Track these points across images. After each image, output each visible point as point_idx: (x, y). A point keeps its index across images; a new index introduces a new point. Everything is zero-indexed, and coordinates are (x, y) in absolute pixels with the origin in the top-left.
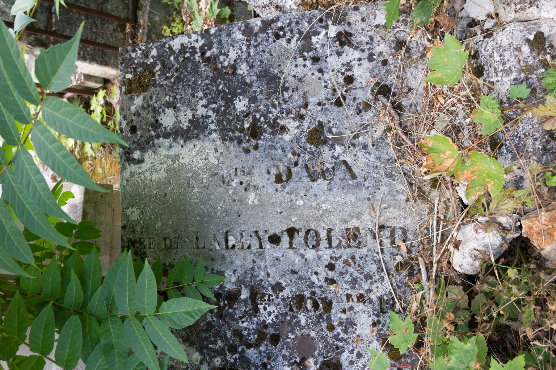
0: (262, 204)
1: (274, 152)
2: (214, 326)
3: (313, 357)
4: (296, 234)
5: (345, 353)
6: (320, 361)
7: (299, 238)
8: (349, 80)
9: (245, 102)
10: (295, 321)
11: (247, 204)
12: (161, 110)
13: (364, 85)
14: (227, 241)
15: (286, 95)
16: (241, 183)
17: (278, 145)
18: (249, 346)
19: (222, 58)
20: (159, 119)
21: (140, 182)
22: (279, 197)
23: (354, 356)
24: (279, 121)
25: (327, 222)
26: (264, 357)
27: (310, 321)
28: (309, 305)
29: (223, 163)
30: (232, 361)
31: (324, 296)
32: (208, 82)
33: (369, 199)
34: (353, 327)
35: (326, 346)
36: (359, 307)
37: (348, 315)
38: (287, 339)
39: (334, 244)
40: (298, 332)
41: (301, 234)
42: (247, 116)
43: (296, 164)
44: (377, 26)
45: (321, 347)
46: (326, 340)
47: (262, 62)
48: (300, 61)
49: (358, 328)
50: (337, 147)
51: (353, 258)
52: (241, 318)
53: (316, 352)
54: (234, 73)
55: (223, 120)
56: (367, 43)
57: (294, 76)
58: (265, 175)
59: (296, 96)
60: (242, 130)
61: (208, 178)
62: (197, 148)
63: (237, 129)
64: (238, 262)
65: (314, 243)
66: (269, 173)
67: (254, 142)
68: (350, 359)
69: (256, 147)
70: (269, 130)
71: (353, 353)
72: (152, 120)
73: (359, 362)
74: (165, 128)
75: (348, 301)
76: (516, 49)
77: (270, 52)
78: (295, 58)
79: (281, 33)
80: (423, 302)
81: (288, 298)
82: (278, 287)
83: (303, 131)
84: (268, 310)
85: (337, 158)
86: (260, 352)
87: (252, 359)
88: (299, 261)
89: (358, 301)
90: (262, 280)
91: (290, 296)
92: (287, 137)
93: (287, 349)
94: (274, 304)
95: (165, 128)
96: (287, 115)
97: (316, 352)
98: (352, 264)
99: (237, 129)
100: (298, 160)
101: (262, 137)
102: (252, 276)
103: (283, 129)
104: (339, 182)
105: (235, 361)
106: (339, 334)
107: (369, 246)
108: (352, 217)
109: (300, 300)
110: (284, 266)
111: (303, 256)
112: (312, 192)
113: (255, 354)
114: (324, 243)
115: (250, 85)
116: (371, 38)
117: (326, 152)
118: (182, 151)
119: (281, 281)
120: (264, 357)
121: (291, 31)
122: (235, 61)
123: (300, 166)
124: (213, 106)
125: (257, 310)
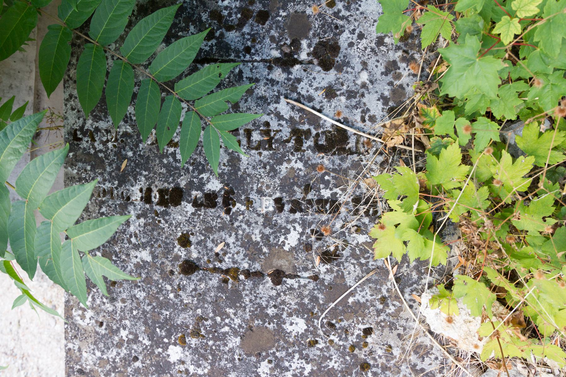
2: (186, 8)
3: (307, 38)
5: (345, 33)
6: (315, 42)
18: (230, 28)
23: (355, 36)
26: (248, 40)
30: (207, 48)
34: (357, 3)
35: (323, 25)
38: (277, 17)
45: (317, 26)
46: (324, 18)
49: (362, 4)
53: (311, 33)
68: (350, 40)
71: (354, 34)
73: (360, 44)
80: (547, 370)
86: (243, 34)
87: (233, 43)
93: (276, 29)
97: (311, 33)
105: (211, 49)
106: (339, 11)
113: (237, 37)
120: (248, 40)
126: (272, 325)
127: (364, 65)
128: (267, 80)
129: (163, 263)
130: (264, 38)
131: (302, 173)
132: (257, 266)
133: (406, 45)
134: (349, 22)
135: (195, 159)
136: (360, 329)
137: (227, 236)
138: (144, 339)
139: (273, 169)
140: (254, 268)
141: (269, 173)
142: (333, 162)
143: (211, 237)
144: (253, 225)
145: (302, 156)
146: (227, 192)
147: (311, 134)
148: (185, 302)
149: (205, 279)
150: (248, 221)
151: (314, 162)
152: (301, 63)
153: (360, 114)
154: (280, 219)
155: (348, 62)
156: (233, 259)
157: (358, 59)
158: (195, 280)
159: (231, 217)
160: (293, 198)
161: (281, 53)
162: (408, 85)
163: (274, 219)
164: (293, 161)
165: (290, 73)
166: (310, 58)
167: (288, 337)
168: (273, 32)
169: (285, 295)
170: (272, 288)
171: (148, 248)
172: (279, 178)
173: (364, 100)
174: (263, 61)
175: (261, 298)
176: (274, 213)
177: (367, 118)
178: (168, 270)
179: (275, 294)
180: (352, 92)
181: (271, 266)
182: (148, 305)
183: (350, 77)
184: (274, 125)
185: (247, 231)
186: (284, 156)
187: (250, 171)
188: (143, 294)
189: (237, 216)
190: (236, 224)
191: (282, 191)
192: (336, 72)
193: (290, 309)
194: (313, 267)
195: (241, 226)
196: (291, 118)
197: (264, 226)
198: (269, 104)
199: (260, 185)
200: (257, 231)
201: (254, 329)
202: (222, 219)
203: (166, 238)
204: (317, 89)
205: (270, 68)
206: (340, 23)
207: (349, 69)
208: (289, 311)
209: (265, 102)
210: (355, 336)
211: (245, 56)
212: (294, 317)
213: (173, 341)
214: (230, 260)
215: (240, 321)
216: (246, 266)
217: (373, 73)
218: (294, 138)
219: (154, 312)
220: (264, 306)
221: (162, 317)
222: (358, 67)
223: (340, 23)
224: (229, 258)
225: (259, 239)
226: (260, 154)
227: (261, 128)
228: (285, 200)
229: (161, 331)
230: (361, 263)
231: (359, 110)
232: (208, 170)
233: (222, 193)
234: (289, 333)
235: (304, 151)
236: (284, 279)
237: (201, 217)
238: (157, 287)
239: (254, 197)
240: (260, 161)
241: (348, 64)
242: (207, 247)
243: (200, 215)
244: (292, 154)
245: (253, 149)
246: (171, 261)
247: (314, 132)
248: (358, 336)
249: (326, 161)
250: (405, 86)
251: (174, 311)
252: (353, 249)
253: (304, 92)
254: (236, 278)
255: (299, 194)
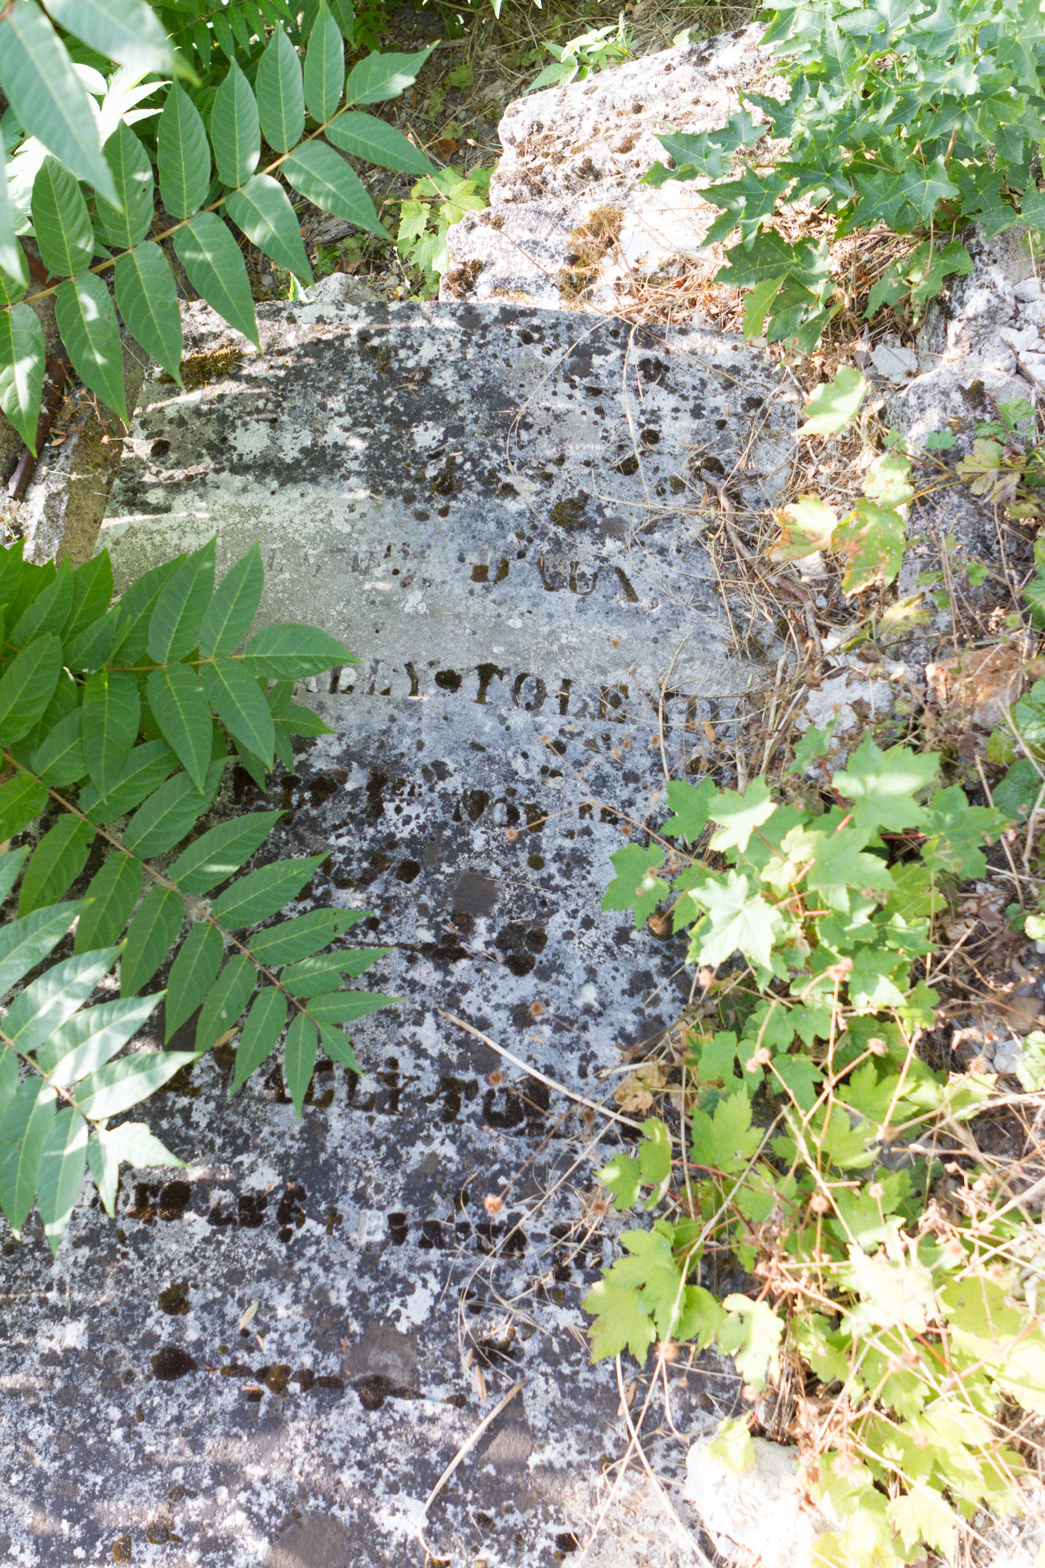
0: (434, 612)
1: (479, 525)
3: (487, 915)
4: (496, 677)
7: (501, 687)
8: (651, 437)
9: (439, 433)
10: (460, 840)
11: (398, 612)
12: (239, 422)
13: (677, 451)
14: (336, 679)
15: (525, 436)
16: (396, 572)
17: (492, 515)
19: (403, 353)
20: (231, 437)
21: (149, 548)
22: (475, 605)
24: (501, 475)
25: (567, 666)
26: (376, 906)
27: (494, 844)
28: (499, 814)
29: (361, 532)
31: (532, 801)
32: (362, 388)
33: (655, 641)
35: (519, 898)
36: (603, 831)
37: (577, 843)
39: (573, 707)
40: (463, 862)
41: (506, 678)
42: (437, 456)
43: (521, 555)
44: (716, 367)
47: (487, 372)
48: (564, 387)
50: (609, 542)
51: (607, 739)
52: (335, 827)
54: (425, 381)
55: (381, 457)
56: (694, 388)
57: (548, 409)
58: (454, 563)
59: (544, 441)
60: (420, 479)
61: (319, 557)
62: (309, 499)
63: (408, 477)
64: (352, 718)
65: (531, 699)
66: (461, 559)
67: (440, 503)
68: (567, 928)
69: (444, 512)
70: (478, 486)
72: (213, 437)
74: (241, 456)
75: (582, 817)
76: (943, 393)
77: (507, 361)
78: (555, 380)
79: (536, 336)
81: (454, 794)
82: (438, 770)
83: (546, 501)
84: (404, 813)
85: (604, 560)
88: (493, 728)
89: (603, 820)
90: (402, 755)
91: (461, 791)
92: (512, 506)
94: (422, 803)
95: (241, 456)
96: (519, 468)
98: (603, 749)
99: (408, 477)
100: (526, 549)
101: (461, 496)
102: (382, 746)
103: (509, 490)
104: (601, 600)
106: (551, 877)
107: (642, 722)
108: (617, 665)
109: (478, 802)
110: (462, 731)
111: (503, 720)
112: (544, 608)
114: (552, 703)
115: (455, 407)
116: (703, 383)
117: (585, 546)
118: (272, 502)
119: (447, 760)
120: (376, 906)
121: (556, 337)
122: (431, 362)
123: (528, 558)
124: (364, 430)
125: (376, 811)
126: (347, 1511)
127: (591, 974)
128: (404, 980)
129: (113, 1353)
130: (406, 906)
131: (452, 1167)
132: (332, 1364)
133: (669, 947)
134: (567, 897)
135: (231, 1124)
136: (549, 1536)
137: (276, 1291)
138: (22, 1551)
139: (393, 1153)
140: (325, 1368)
141: (384, 1160)
142: (518, 1149)
143: (238, 1294)
144: (337, 1268)
145: (457, 1131)
146: (290, 1195)
147: (477, 1089)
148: (148, 1449)
149: (207, 1393)
150: (326, 1258)
151: (479, 1145)
152: (471, 957)
153: (577, 1062)
154: (396, 1260)
155: (562, 966)
156: (280, 1343)
157: (579, 962)
158: (183, 1393)
159: (290, 1249)
160: (429, 1218)
161: (436, 936)
162: (671, 1018)
163: (384, 1258)
164: (437, 1142)
165: (448, 972)
166: (491, 950)
167: (382, 1545)
168: (424, 898)
169: (388, 1437)
170: (359, 1419)
171: (85, 1317)
172: (404, 1172)
173: (587, 1036)
174: (401, 946)
175: (331, 1442)
176: (384, 1245)
177: (590, 1070)
178: (123, 1369)
179: (363, 1435)
180: (565, 1019)
181: (364, 1365)
182: (54, 1459)
183: (562, 991)
184: (407, 1065)
185: (322, 1280)
186: (419, 1127)
187: (345, 1152)
188: (48, 1431)
189: (304, 1247)
190: (300, 1265)
191: (407, 1200)
192: (536, 981)
193: (394, 1473)
194: (458, 1375)
195: (309, 1269)
196: (442, 1056)
197: (361, 1272)
198: (401, 1025)
199: (362, 1183)
200: (342, 1284)
201: (305, 1520)
202: (270, 1253)
203: (133, 1293)
204: (497, 1007)
205: (412, 960)
206: (550, 896)
207: (562, 978)
208: (392, 1478)
209: (393, 1020)
210: (536, 1554)
211: (365, 934)
212: (402, 1494)
213: (97, 1555)
214: (274, 1347)
215: (273, 1497)
216: (307, 1361)
217: (607, 988)
218: (443, 1094)
219: (65, 1476)
220: (336, 1462)
221: (83, 1490)
222: (580, 976)
223: (550, 896)
224: (272, 1342)
225: (344, 1302)
226: (371, 1120)
227: (380, 1070)
228: (409, 1221)
229: (71, 1527)
230: (560, 1373)
231: (577, 1054)
232: (256, 1147)
233: (280, 1195)
234: (385, 1536)
235: (461, 1122)
236: (389, 1399)
237: (223, 1248)
238: (85, 1412)
239: (346, 1208)
240: (369, 1134)
241: (560, 969)
242: (224, 1316)
243: (222, 1242)
244: (436, 1125)
245: (357, 1108)
246: (132, 1349)
247: (484, 1087)
248: (545, 1552)
249: (504, 1149)
250: (665, 1018)
251: (115, 1474)
252: (547, 1341)
253: (471, 1011)
254: (279, 1388)
255: (441, 1212)
